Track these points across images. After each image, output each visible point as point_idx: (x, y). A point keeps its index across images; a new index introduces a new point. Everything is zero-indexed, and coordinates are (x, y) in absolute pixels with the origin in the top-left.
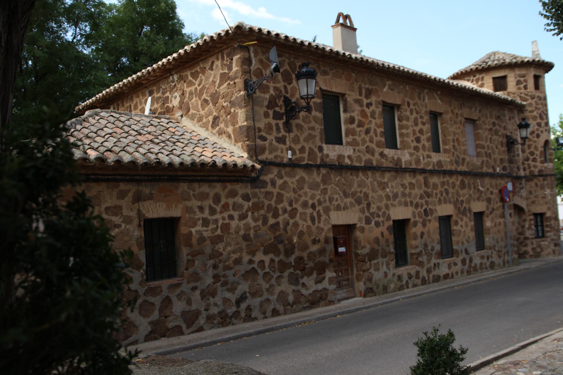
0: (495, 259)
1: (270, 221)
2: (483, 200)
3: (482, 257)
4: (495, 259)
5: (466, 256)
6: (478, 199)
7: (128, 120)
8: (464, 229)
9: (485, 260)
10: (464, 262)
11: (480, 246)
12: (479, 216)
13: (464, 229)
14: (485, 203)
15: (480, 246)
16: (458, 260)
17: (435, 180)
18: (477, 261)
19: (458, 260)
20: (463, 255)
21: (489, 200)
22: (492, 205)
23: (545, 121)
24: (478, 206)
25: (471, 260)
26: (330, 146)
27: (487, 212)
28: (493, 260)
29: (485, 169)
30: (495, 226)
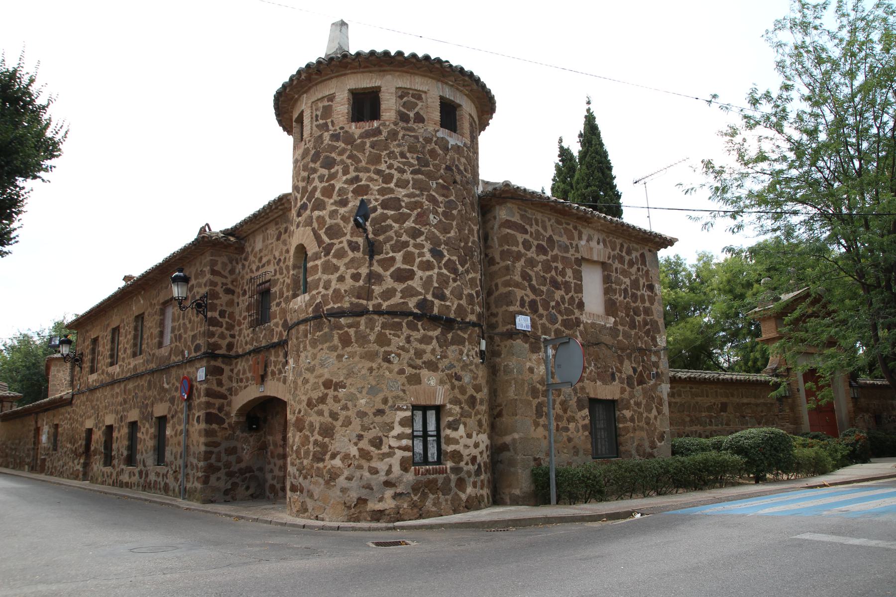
0: (170, 481)
1: (415, 285)
2: (166, 401)
3: (158, 474)
4: (170, 481)
5: (143, 468)
6: (161, 400)
7: (781, 171)
8: (146, 434)
9: (160, 479)
10: (141, 473)
11: (160, 459)
12: (162, 421)
13: (146, 434)
14: (168, 404)
15: (160, 459)
16: (136, 470)
17: (131, 386)
18: (152, 477)
19: (136, 470)
20: (141, 467)
21: (172, 400)
22: (175, 407)
23: (802, 450)
24: (160, 410)
25: (147, 475)
26: (50, 393)
27: (169, 416)
28: (168, 481)
29: (175, 359)
30: (176, 435)
